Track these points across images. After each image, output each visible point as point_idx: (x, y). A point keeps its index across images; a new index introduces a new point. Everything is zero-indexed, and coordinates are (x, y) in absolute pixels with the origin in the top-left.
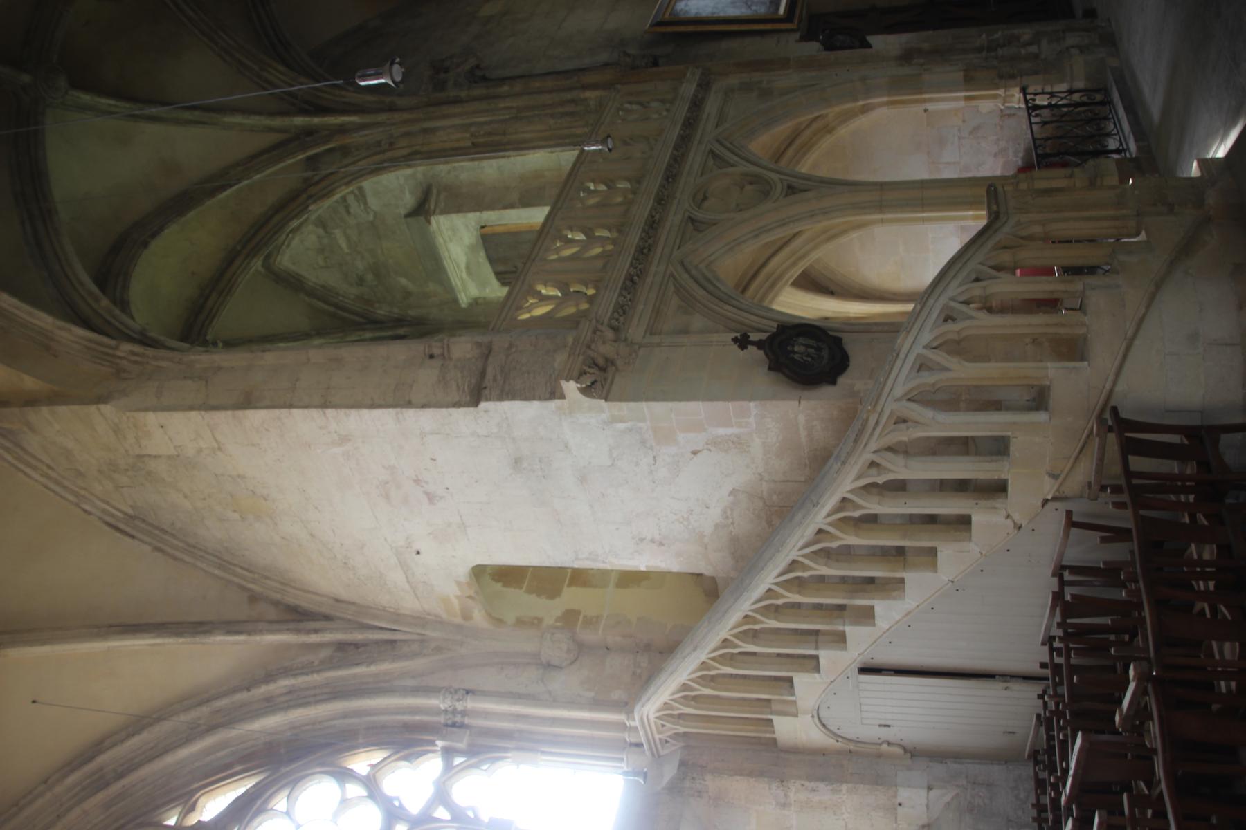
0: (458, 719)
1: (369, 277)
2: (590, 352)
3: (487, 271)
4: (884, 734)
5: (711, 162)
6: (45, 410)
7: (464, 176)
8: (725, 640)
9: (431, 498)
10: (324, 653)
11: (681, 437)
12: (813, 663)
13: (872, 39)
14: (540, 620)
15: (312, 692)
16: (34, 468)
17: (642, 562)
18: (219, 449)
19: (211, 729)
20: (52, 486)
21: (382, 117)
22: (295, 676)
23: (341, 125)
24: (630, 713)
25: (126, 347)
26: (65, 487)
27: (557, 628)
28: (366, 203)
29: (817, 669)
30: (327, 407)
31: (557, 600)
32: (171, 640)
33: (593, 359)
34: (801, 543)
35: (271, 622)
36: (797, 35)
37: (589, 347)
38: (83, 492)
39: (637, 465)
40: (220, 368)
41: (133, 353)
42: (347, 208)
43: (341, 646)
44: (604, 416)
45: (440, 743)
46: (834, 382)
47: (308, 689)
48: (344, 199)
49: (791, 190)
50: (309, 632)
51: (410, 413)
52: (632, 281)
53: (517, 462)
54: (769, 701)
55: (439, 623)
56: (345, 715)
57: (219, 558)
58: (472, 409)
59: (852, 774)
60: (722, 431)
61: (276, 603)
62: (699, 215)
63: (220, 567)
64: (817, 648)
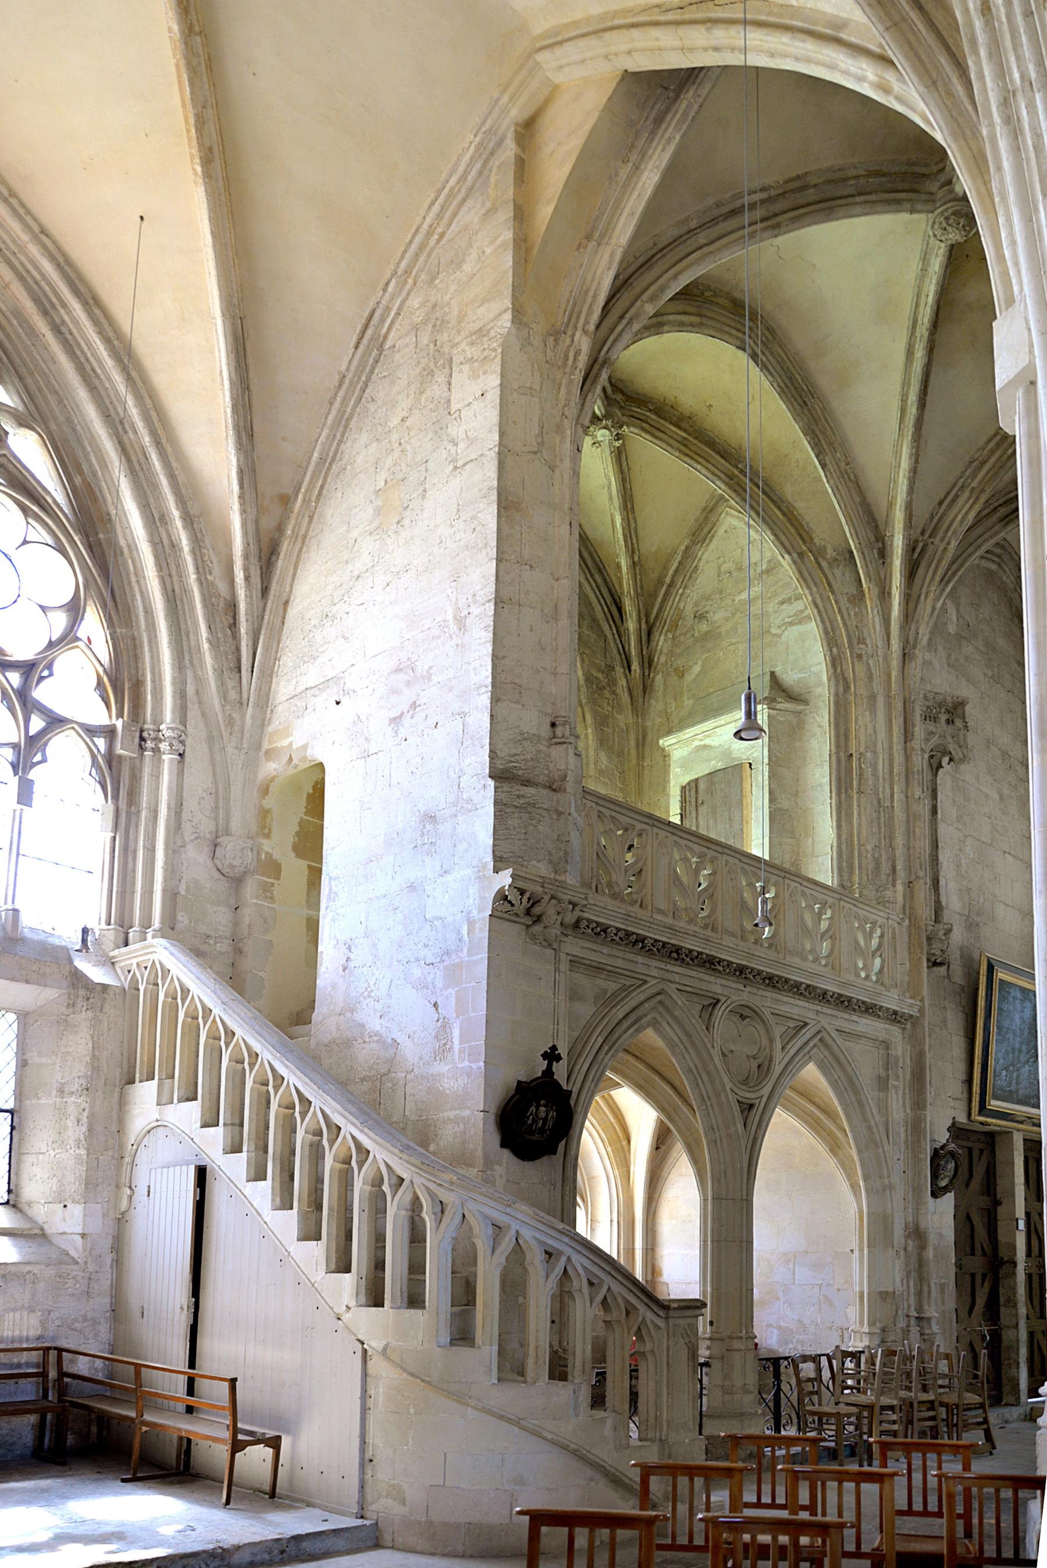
0: (149, 744)
1: (704, 627)
2: (547, 898)
3: (700, 771)
4: (141, 1191)
5: (792, 1024)
6: (508, 235)
7: (814, 743)
8: (234, 1034)
9: (396, 721)
10: (222, 587)
11: (452, 992)
12: (210, 1121)
13: (949, 1198)
14: (268, 836)
15: (174, 573)
16: (439, 216)
17: (326, 947)
18: (456, 468)
19: (124, 450)
20: (418, 240)
21: (896, 644)
22: (193, 551)
23: (889, 594)
24: (162, 933)
25: (584, 344)
26: (417, 256)
27: (259, 854)
28: (791, 624)
29: (205, 1125)
30: (496, 604)
31: (293, 854)
32: (228, 399)
33: (539, 901)
34: (326, 1109)
35: (257, 522)
36: (962, 1119)
37: (553, 897)
38: (410, 281)
39: (426, 946)
40: (552, 468)
41: (577, 353)
42: (787, 601)
43: (232, 606)
44: (475, 913)
45: (119, 724)
46: (503, 1145)
47: (178, 567)
48: (798, 598)
49: (747, 1108)
50: (246, 569)
51: (484, 700)
52: (636, 941)
53: (431, 818)
54: (173, 1077)
55: (262, 723)
56: (149, 612)
57: (334, 458)
58: (487, 771)
59: (97, 1159)
60: (456, 1033)
61: (280, 529)
62: (719, 1012)
63: (322, 460)
64: (225, 1125)
